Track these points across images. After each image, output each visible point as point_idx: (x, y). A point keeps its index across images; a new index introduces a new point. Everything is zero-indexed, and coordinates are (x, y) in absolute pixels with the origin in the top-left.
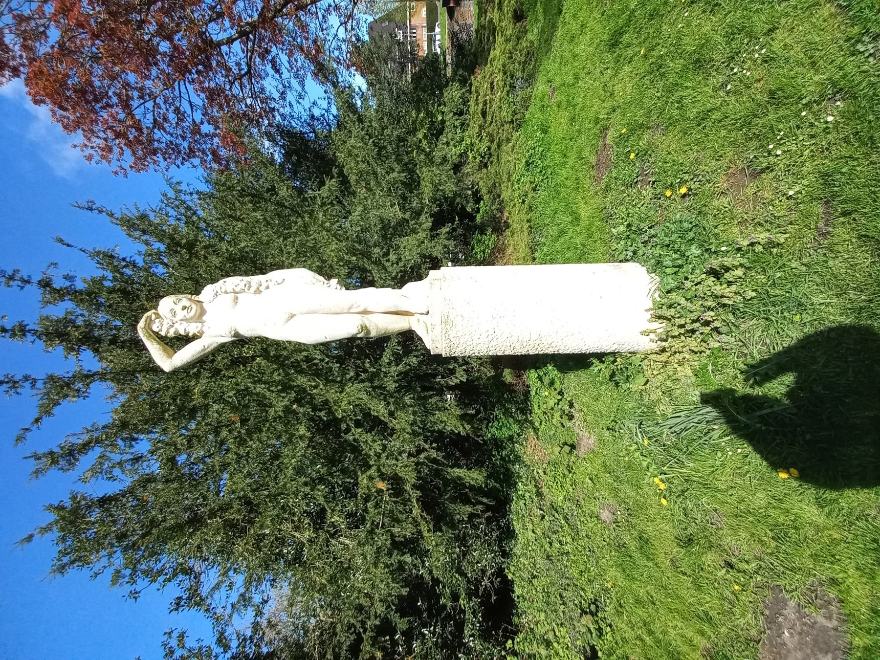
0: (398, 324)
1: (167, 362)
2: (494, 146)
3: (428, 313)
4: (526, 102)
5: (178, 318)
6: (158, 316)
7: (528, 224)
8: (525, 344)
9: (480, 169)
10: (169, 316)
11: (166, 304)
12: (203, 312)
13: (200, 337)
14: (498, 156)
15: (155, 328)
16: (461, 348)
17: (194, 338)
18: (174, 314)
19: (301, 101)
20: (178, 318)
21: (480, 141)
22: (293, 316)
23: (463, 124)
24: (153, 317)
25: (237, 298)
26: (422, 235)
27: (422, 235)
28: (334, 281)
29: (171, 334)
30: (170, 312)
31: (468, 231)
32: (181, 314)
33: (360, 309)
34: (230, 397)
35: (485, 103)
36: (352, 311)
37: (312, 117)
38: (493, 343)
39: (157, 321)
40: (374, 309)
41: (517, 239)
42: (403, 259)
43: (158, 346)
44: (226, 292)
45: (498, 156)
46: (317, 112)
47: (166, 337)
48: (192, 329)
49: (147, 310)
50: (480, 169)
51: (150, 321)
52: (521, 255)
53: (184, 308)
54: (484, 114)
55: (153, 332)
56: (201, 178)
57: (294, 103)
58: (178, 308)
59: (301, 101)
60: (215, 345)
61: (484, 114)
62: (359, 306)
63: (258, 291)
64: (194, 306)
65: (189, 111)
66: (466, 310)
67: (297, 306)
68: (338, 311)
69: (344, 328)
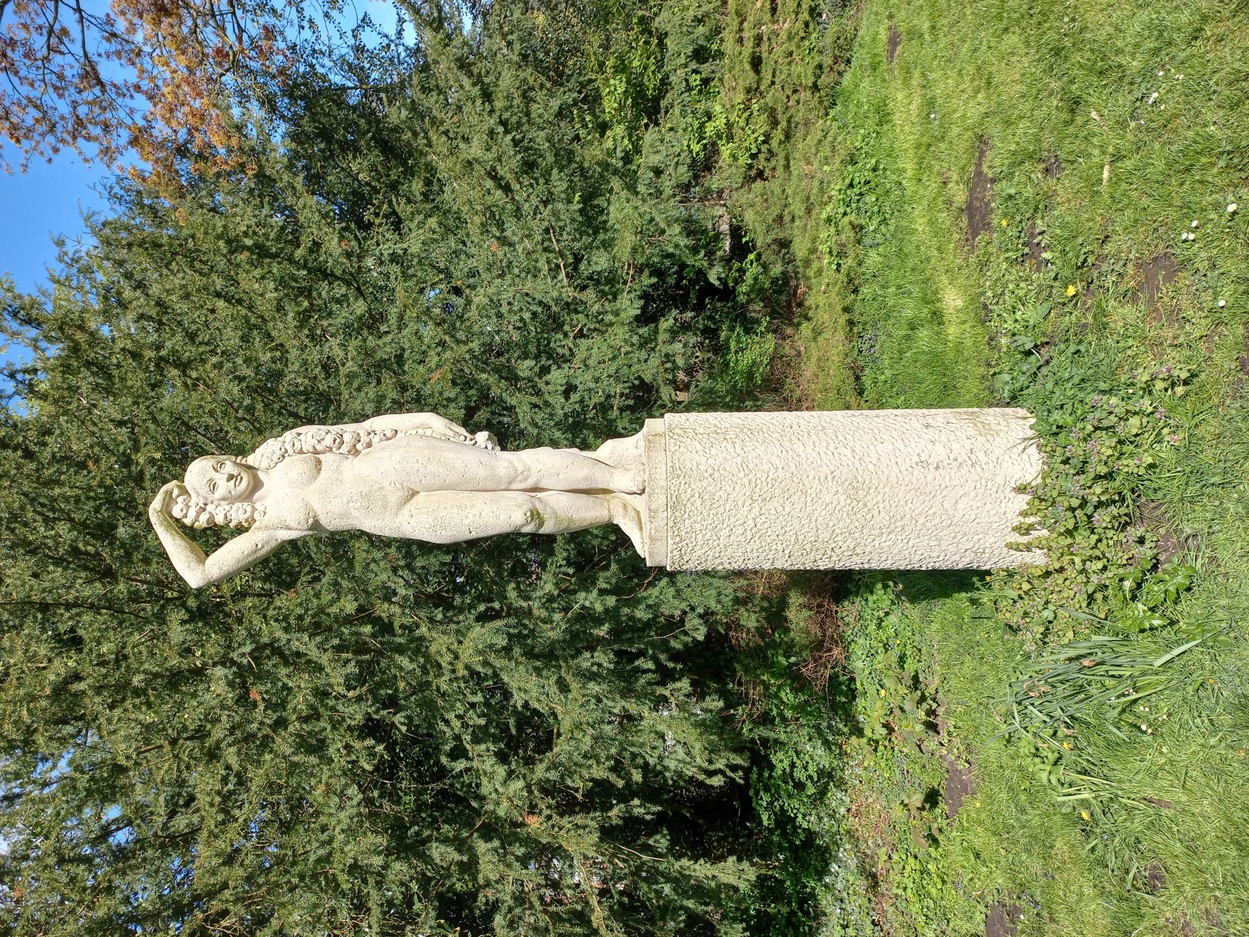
0: (587, 513)
1: (194, 572)
2: (778, 135)
3: (643, 491)
4: (842, 56)
5: (220, 493)
6: (184, 491)
7: (847, 316)
8: (808, 547)
9: (749, 180)
10: (205, 491)
11: (198, 471)
12: (257, 485)
13: (247, 530)
14: (787, 159)
15: (177, 512)
16: (699, 553)
17: (240, 530)
18: (213, 486)
19: (334, 13)
20: (220, 493)
21: (747, 121)
22: (414, 493)
23: (706, 82)
24: (176, 492)
25: (319, 462)
26: (619, 335)
27: (619, 335)
28: (482, 436)
29: (202, 522)
30: (204, 485)
31: (723, 321)
32: (223, 487)
33: (530, 483)
34: (243, 655)
35: (759, 39)
36: (514, 486)
37: (359, 49)
38: (753, 546)
39: (180, 499)
40: (537, 486)
41: (821, 345)
42: (580, 387)
43: (183, 543)
44: (301, 452)
45: (787, 159)
46: (371, 40)
47: (192, 528)
48: (238, 514)
49: (165, 482)
50: (749, 180)
51: (169, 497)
52: (833, 382)
53: (231, 477)
54: (756, 63)
55: (172, 517)
56: (100, 188)
57: (319, 20)
58: (221, 478)
59: (334, 13)
60: (273, 544)
61: (756, 63)
62: (526, 479)
63: (354, 452)
64: (244, 475)
65: (75, 30)
66: (715, 491)
67: (409, 477)
68: (490, 485)
69: (499, 515)
